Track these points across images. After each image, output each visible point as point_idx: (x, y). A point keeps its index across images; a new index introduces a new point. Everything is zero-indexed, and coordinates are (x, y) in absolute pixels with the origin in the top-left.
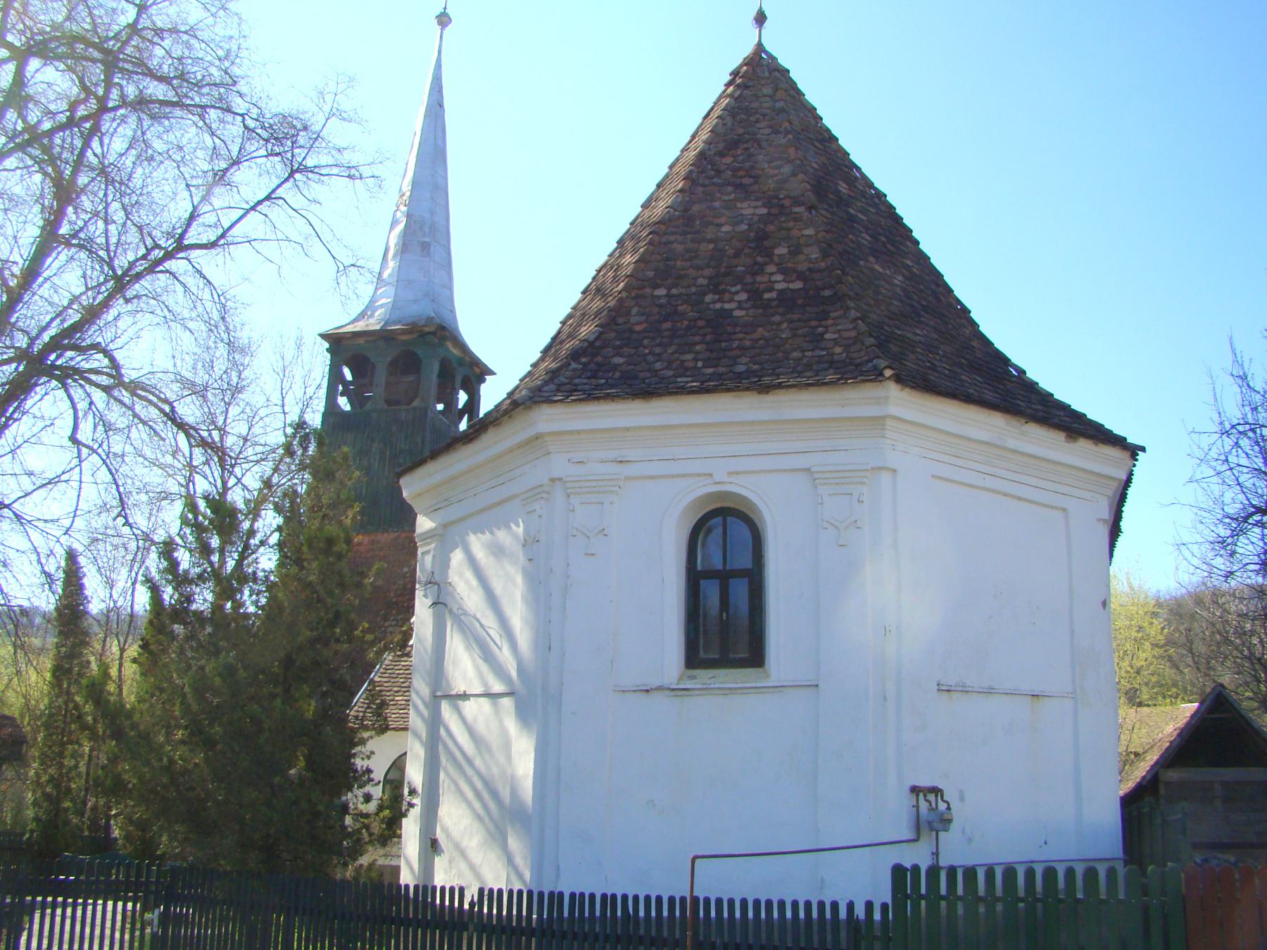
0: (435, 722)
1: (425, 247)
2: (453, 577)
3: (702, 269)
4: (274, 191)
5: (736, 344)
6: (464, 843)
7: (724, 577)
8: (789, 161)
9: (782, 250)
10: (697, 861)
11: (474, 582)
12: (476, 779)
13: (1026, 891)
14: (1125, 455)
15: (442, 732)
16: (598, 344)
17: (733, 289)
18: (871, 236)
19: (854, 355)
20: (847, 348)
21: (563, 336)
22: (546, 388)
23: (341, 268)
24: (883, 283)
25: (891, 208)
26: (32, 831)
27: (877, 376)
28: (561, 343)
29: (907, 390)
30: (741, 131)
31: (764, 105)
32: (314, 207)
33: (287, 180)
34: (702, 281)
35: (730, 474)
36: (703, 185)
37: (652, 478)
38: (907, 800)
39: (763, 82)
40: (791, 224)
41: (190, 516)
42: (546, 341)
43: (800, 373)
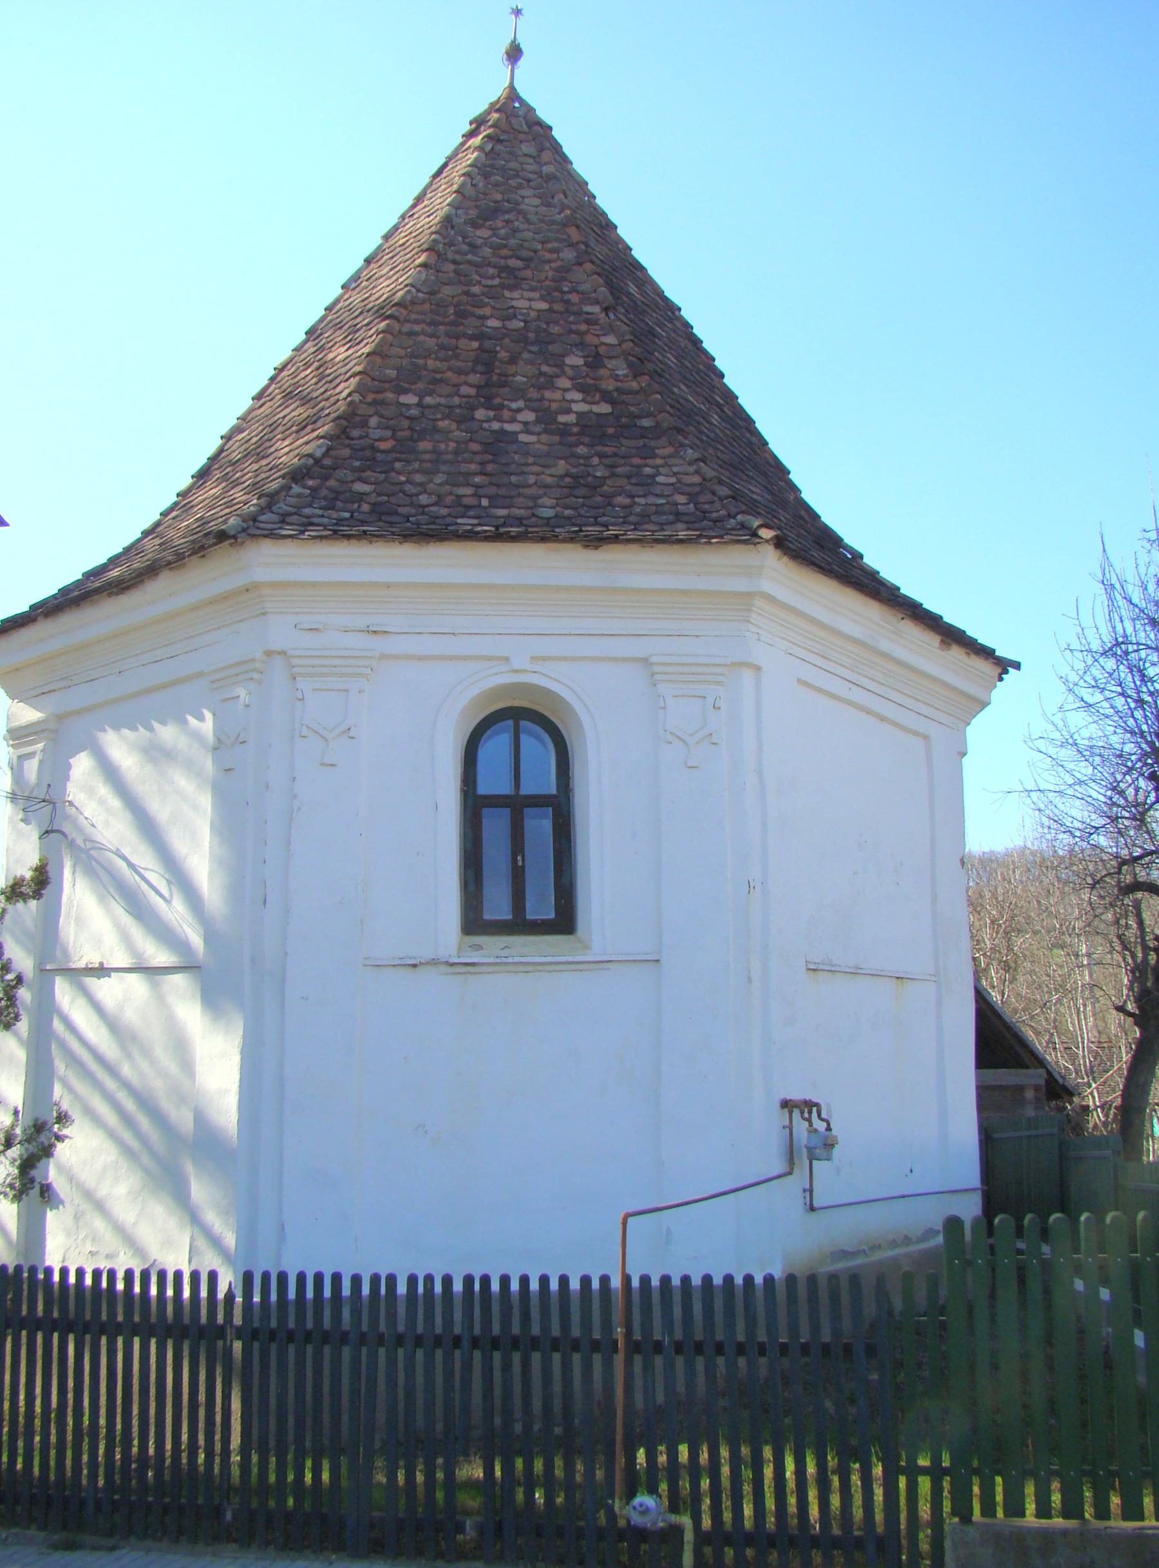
2: (74, 792)
3: (467, 374)
5: (532, 479)
6: (102, 1191)
7: (517, 805)
10: (630, 1220)
11: (115, 803)
12: (122, 1096)
15: (57, 1025)
17: (514, 405)
20: (692, 498)
22: (262, 518)
25: (688, 326)
27: (752, 537)
29: (785, 559)
30: (499, 197)
36: (454, 262)
37: (420, 658)
40: (583, 327)
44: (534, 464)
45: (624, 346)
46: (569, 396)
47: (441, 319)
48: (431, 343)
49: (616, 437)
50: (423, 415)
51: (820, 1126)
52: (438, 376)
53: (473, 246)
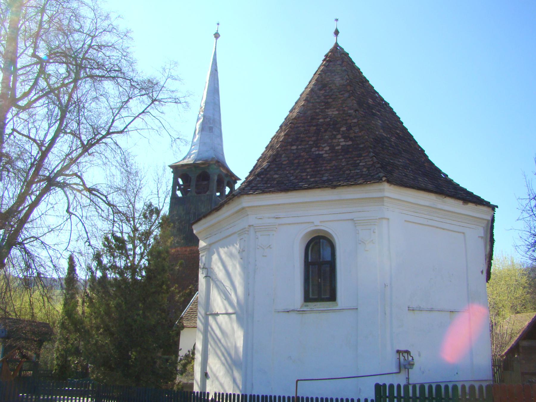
0: (206, 324)
1: (211, 129)
4: (145, 109)
5: (323, 168)
6: (217, 374)
8: (348, 92)
9: (343, 129)
10: (299, 382)
13: (420, 394)
14: (490, 210)
15: (209, 328)
16: (268, 169)
17: (324, 146)
19: (371, 172)
20: (368, 169)
21: (257, 166)
22: (246, 189)
24: (386, 141)
26: (56, 370)
29: (392, 186)
32: (162, 115)
33: (151, 104)
34: (311, 143)
35: (321, 222)
37: (289, 224)
40: (347, 118)
41: (106, 243)
48: (302, 129)
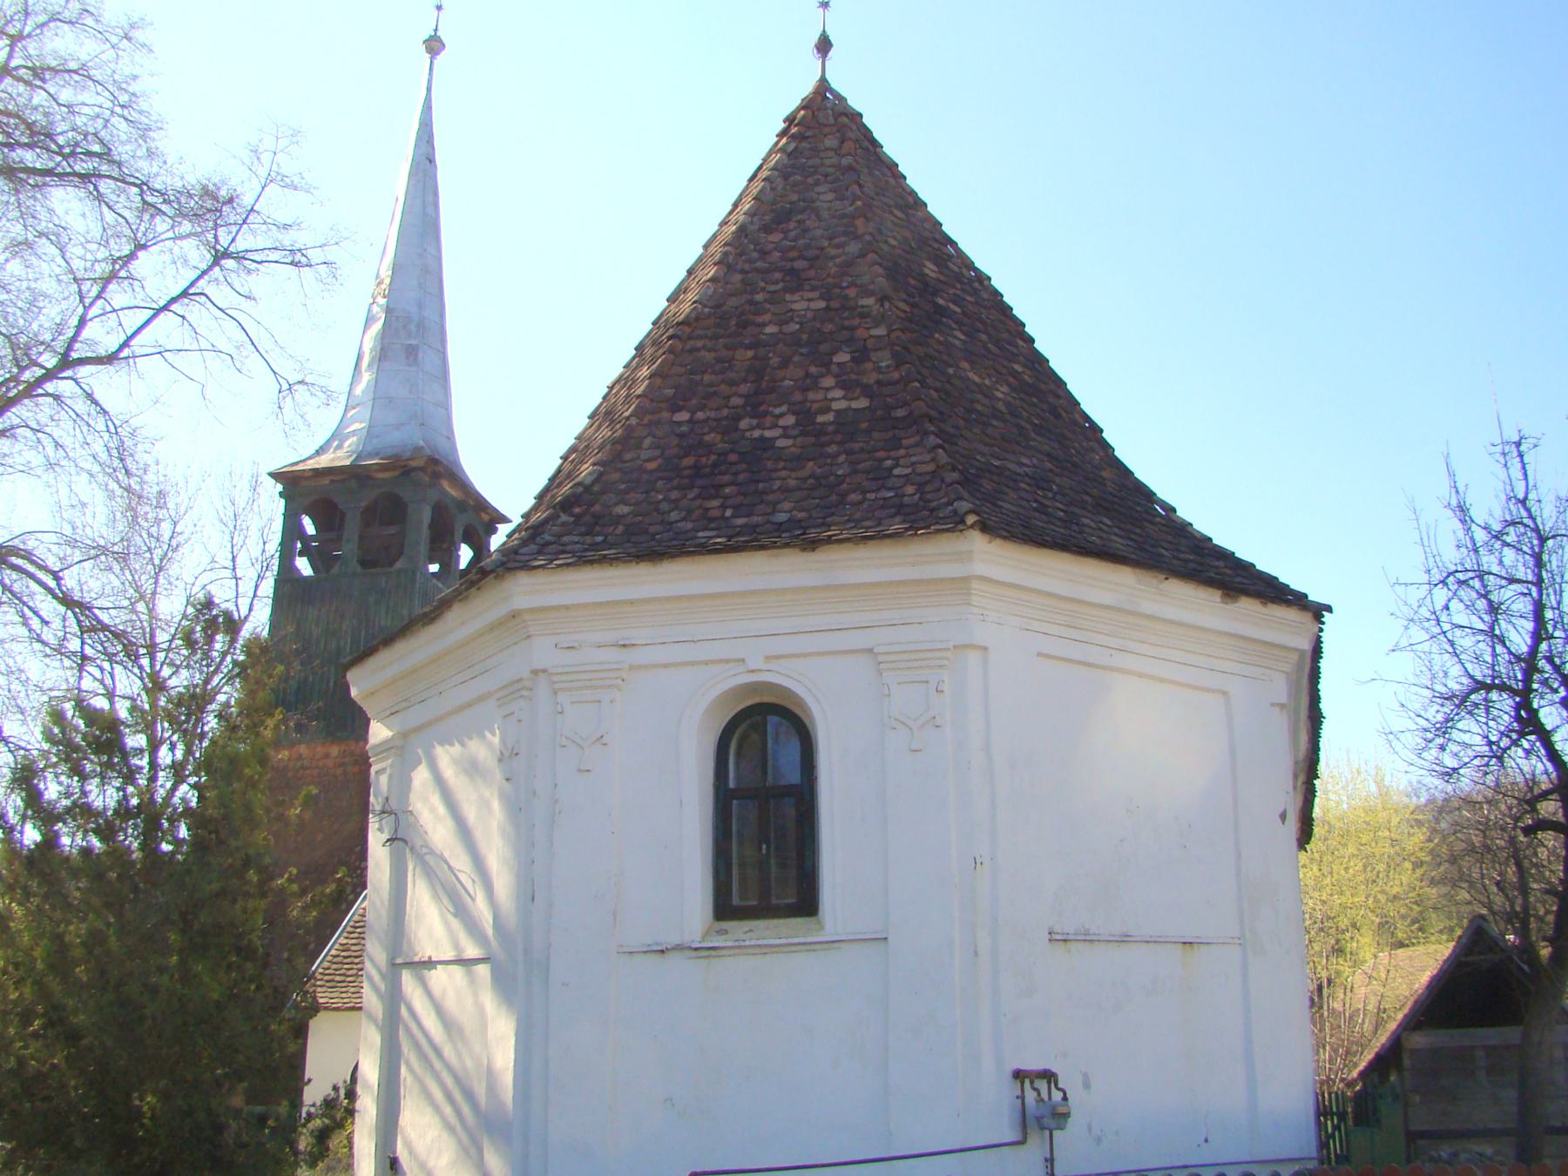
0: (394, 998)
1: (412, 352)
3: (738, 384)
4: (192, 284)
5: (777, 484)
9: (843, 357)
11: (442, 810)
14: (1307, 618)
15: (404, 1011)
16: (596, 488)
17: (777, 411)
18: (965, 334)
19: (929, 496)
20: (920, 487)
23: (285, 386)
25: (997, 295)
28: (559, 485)
29: (998, 541)
30: (795, 197)
31: (827, 162)
33: (210, 268)
35: (768, 658)
36: (743, 272)
37: (665, 666)
38: (1009, 1089)
39: (827, 130)
41: (56, 730)
42: (542, 482)
43: (858, 521)
44: (784, 468)
45: (893, 336)
46: (831, 395)
47: (721, 331)
48: (709, 357)
49: (868, 431)
50: (692, 430)
51: (1057, 1096)
52: (712, 390)
53: (764, 253)
